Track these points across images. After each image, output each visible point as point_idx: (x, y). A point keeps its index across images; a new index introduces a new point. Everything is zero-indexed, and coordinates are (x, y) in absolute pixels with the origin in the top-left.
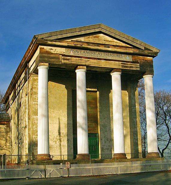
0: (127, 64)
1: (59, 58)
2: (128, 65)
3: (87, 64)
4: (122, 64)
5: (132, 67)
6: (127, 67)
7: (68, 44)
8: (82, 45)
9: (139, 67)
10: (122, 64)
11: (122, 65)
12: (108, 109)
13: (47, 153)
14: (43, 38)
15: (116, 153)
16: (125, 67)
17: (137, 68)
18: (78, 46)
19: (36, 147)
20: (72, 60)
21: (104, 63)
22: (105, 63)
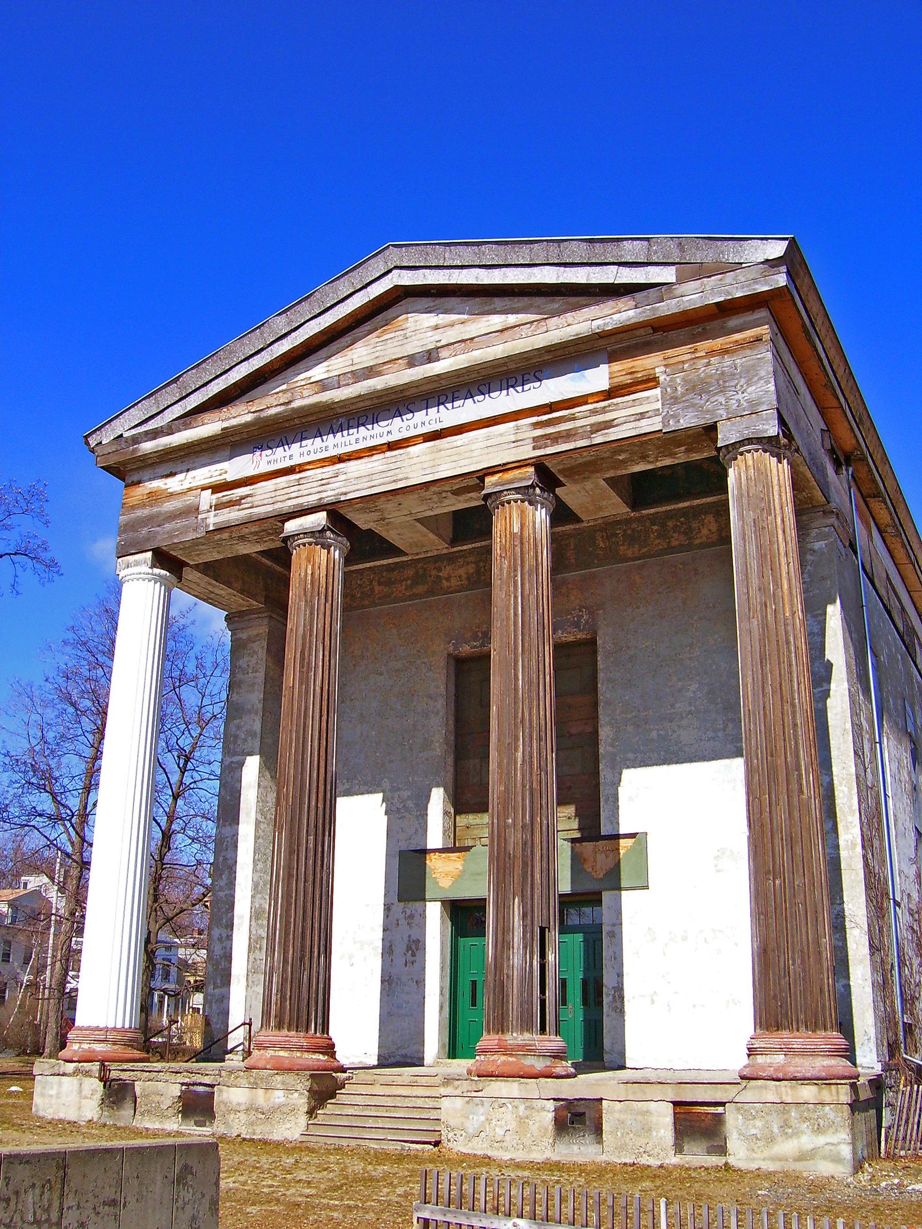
0: (573, 418)
1: (195, 510)
2: (579, 423)
3: (329, 495)
4: (536, 425)
5: (608, 425)
6: (568, 436)
7: (226, 424)
8: (289, 402)
9: (657, 412)
10: (536, 425)
11: (539, 432)
12: (654, 734)
13: (127, 1026)
14: (121, 436)
15: (86, 1024)
16: (555, 438)
17: (644, 422)
18: (273, 411)
19: (223, 990)
20: (256, 500)
21: (423, 458)
22: (427, 458)
